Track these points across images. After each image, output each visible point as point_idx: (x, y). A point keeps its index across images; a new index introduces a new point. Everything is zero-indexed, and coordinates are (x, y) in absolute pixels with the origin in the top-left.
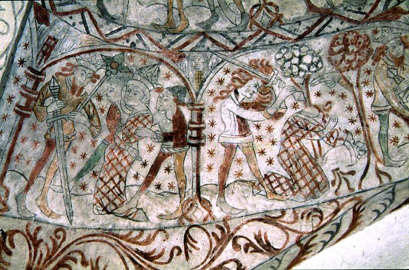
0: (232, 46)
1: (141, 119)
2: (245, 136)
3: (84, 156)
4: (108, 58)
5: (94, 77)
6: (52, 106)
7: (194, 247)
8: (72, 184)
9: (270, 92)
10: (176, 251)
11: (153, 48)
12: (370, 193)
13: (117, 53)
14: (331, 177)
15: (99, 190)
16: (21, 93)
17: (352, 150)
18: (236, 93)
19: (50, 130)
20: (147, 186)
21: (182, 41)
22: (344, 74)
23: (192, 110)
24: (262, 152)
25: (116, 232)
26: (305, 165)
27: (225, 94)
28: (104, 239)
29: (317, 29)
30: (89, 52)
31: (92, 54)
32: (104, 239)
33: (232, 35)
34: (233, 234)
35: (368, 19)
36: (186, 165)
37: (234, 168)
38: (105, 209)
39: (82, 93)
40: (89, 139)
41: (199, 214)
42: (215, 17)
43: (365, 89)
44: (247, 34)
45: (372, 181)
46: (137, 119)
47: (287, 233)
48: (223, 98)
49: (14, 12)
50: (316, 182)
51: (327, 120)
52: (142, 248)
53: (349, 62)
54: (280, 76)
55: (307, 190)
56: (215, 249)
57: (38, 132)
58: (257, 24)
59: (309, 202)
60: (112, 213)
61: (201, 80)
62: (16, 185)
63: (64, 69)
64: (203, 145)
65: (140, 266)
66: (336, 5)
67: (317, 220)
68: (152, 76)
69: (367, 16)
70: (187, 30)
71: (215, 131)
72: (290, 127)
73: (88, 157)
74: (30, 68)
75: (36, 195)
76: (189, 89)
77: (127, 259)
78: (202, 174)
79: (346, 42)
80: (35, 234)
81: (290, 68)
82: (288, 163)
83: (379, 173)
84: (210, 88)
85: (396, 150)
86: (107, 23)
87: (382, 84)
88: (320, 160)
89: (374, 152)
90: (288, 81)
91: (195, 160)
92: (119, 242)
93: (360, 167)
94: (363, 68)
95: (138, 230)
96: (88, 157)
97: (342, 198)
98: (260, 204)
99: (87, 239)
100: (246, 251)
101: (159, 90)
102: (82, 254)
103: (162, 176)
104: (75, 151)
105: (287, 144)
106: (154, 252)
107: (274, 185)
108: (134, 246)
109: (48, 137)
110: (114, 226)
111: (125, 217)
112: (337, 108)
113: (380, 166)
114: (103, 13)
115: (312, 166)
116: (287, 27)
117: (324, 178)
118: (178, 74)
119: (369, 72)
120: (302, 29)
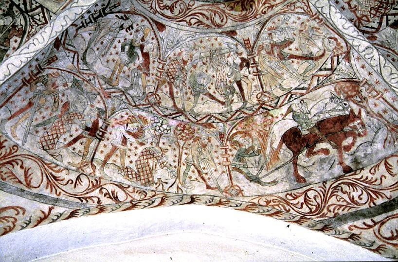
0: (134, 104)
1: (78, 114)
2: (124, 145)
3: (44, 118)
4: (76, 79)
5: (65, 85)
6: (40, 87)
7: (80, 183)
8: (32, 127)
9: (142, 132)
10: (70, 182)
11: (98, 86)
12: (171, 195)
13: (81, 80)
14: (156, 181)
15: (44, 137)
16: (29, 74)
17: (170, 173)
18: (127, 125)
19: (34, 97)
20: (68, 146)
21: (112, 90)
22: (178, 140)
23: (104, 123)
24: (129, 157)
25: (44, 160)
26: (146, 170)
27: (121, 123)
28: (37, 160)
29: (174, 116)
30: (69, 72)
31: (70, 74)
32: (37, 160)
33: (135, 100)
34: (101, 186)
35: (197, 123)
36: (91, 145)
37: (113, 157)
38: (43, 147)
39: (57, 89)
40: (49, 111)
41: (88, 170)
42: (131, 87)
43: (185, 151)
44: (143, 102)
45: (174, 190)
46: (76, 114)
47: (127, 196)
48: (120, 124)
49: (50, 36)
50: (149, 180)
51: (163, 156)
52: (54, 173)
53: (183, 136)
54: (150, 128)
55: (143, 182)
56: (90, 189)
57: (28, 96)
58: (149, 101)
59: (142, 187)
60: (46, 150)
61: (113, 112)
62: (4, 114)
63: (54, 73)
64: (103, 140)
65: (50, 181)
66: (186, 110)
67: (143, 196)
68: (92, 98)
69: (197, 121)
70: (117, 87)
71: (111, 137)
72: (146, 152)
73: (46, 119)
74: (39, 64)
75: (12, 124)
76: (106, 113)
77: (44, 175)
78: (97, 153)
79: (184, 127)
80: (3, 142)
81: (156, 126)
82: (139, 166)
83: (178, 188)
84: (117, 117)
85: (189, 181)
86: (83, 64)
87: (193, 152)
88: (154, 171)
89: (179, 178)
90: (152, 132)
91: (96, 144)
92: (43, 165)
93: (171, 182)
94: (187, 142)
95: (55, 164)
96: (46, 119)
97: (158, 191)
98: (120, 178)
99: (28, 157)
100: (105, 196)
101: (92, 106)
102: (22, 163)
103: (77, 145)
104: (40, 113)
105: (142, 158)
106: (59, 177)
107: (129, 173)
108: (50, 171)
109: (31, 100)
110: (44, 157)
111: (52, 155)
112: (170, 153)
113: (180, 186)
114: (84, 59)
115: (149, 172)
116: (161, 109)
117: (153, 180)
118: (104, 103)
119: (189, 145)
120: (167, 113)
